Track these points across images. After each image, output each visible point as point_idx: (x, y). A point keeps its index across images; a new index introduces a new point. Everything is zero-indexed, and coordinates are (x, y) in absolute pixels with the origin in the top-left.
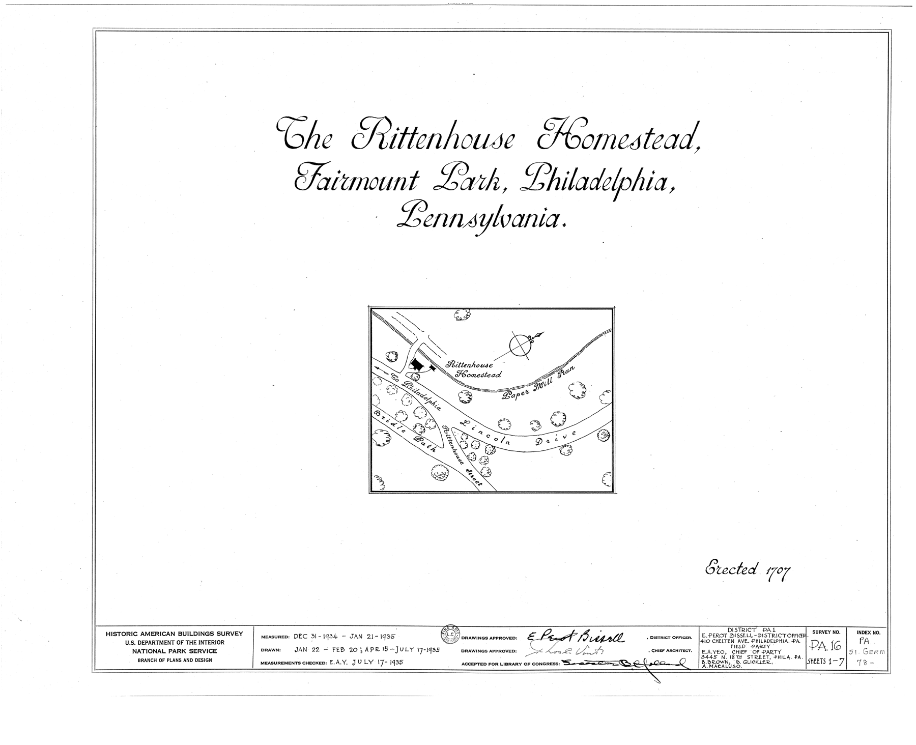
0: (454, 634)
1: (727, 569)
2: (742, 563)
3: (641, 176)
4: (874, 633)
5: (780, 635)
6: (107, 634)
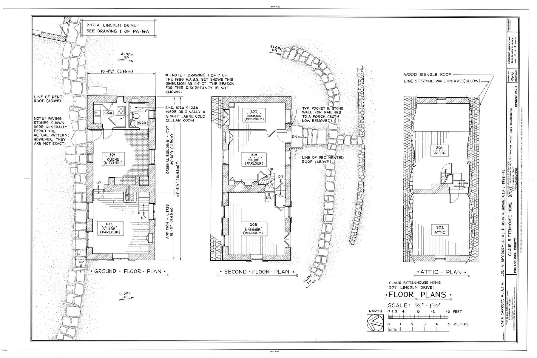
6: (510, 212)
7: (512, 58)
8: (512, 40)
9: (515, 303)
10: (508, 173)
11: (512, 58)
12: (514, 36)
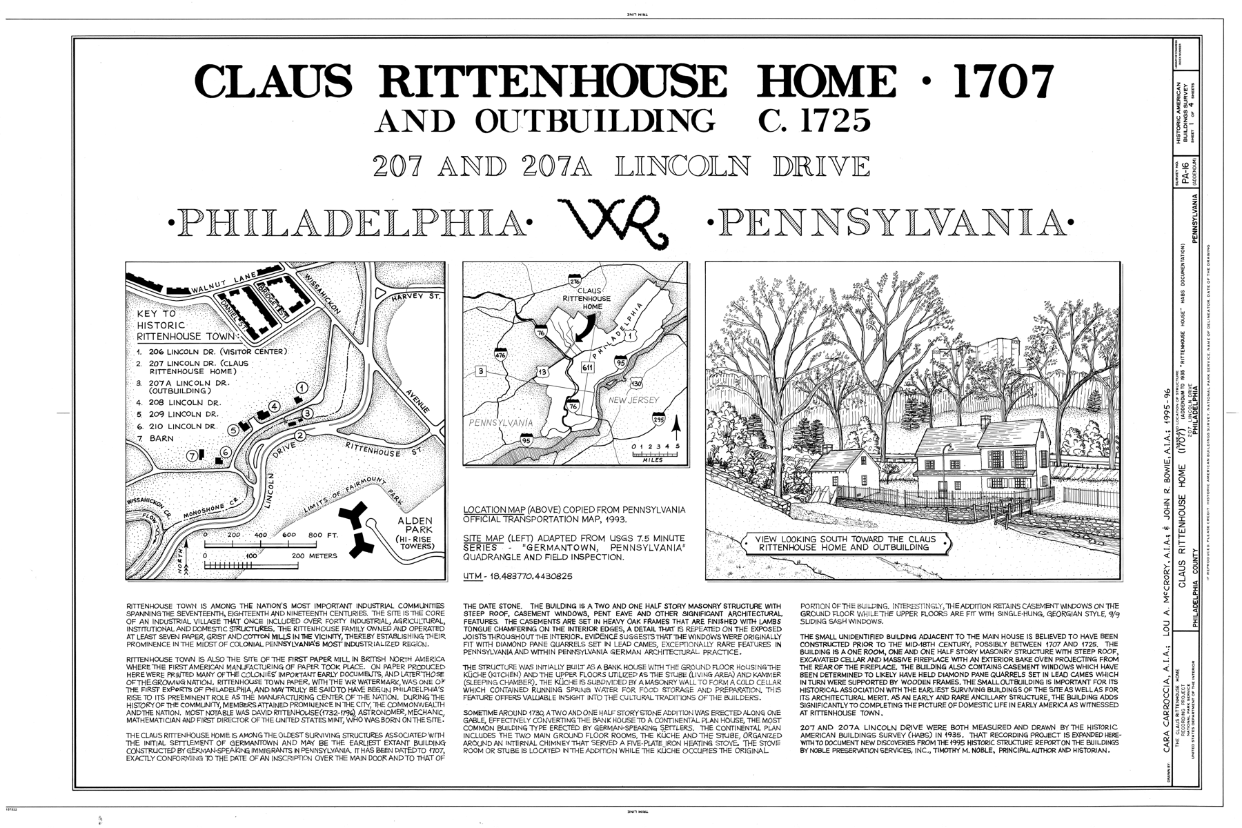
7: (185, 391)
8: (1185, 90)
11: (185, 391)
12: (1190, 79)
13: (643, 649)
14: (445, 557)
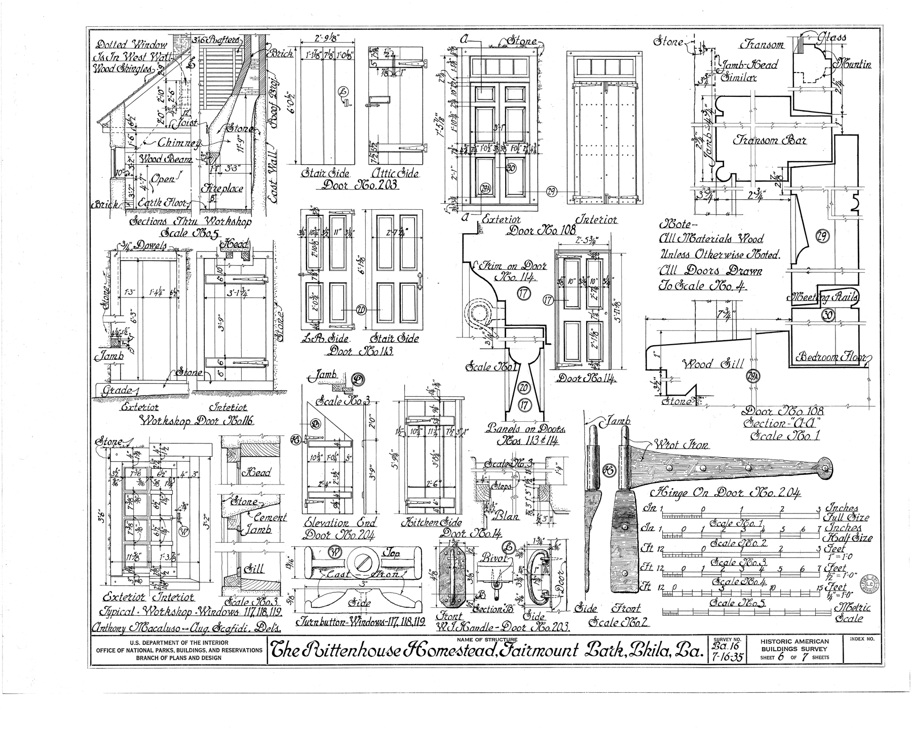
0: (873, 584)
1: (299, 649)
2: (578, 644)
3: (680, 649)
4: (405, 339)
5: (113, 469)
7: (776, 649)
8: (820, 649)
9: (160, 662)
10: (189, 643)
12: (833, 651)
13: (224, 416)
14: (733, 340)
